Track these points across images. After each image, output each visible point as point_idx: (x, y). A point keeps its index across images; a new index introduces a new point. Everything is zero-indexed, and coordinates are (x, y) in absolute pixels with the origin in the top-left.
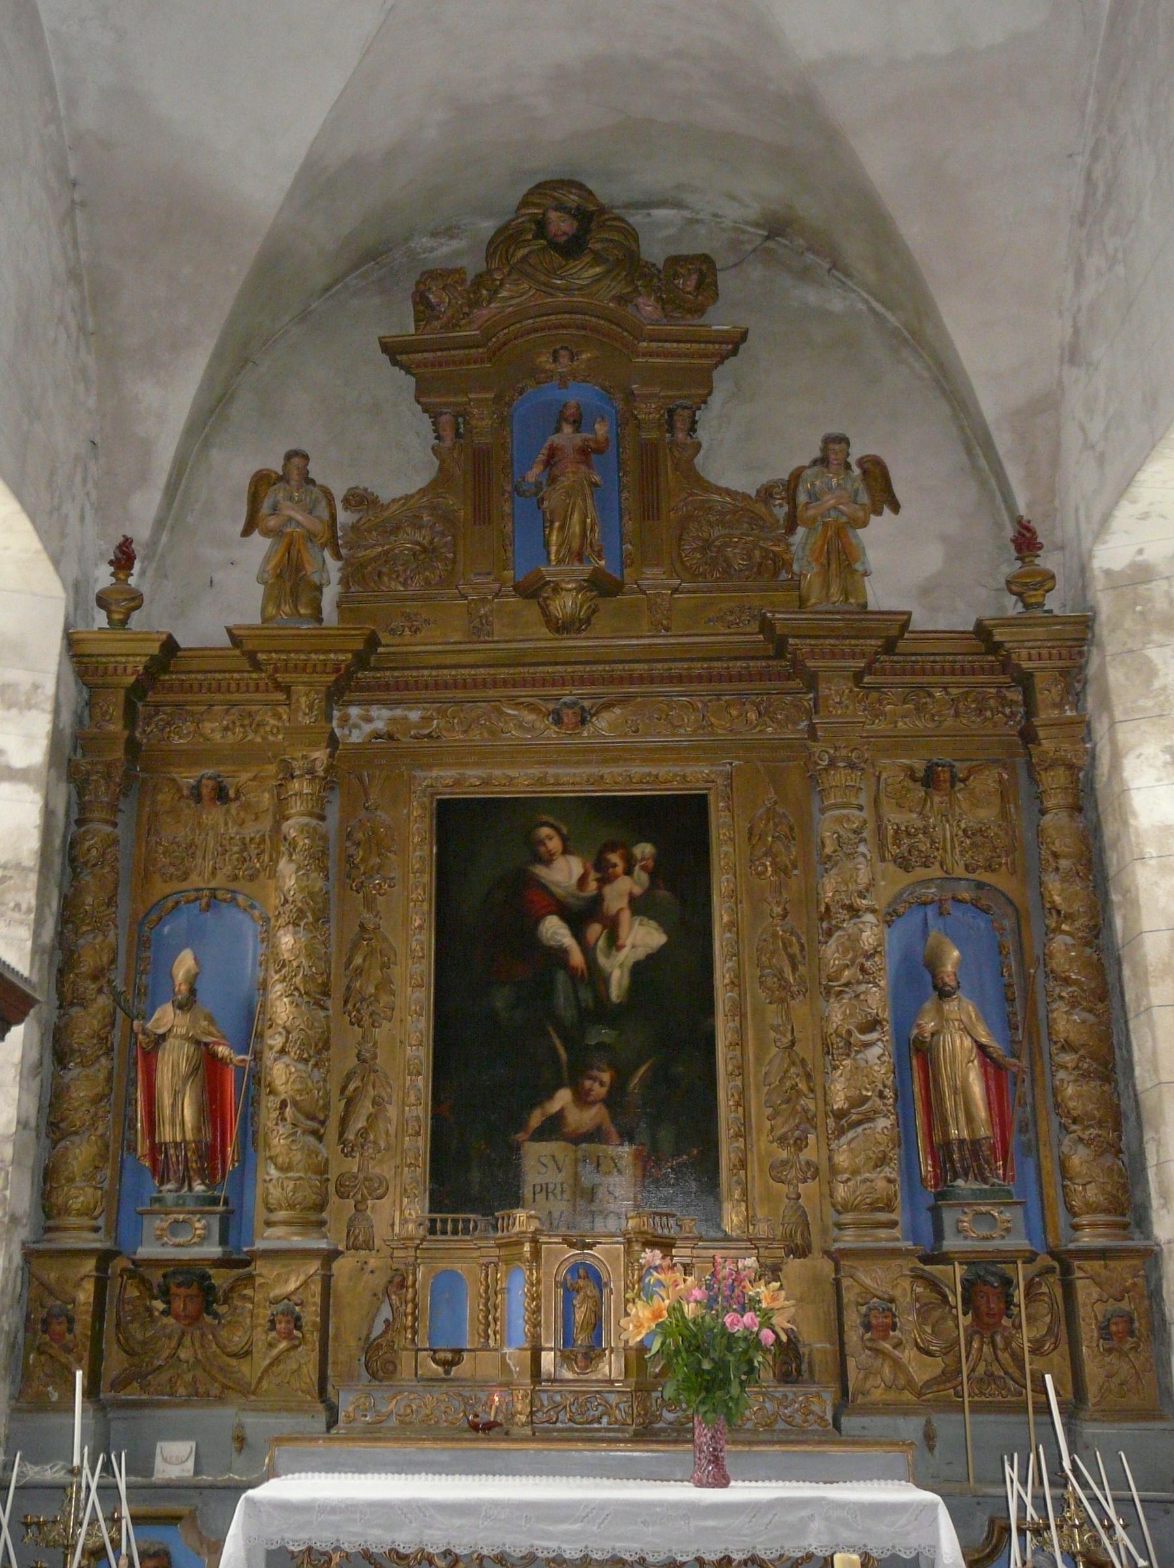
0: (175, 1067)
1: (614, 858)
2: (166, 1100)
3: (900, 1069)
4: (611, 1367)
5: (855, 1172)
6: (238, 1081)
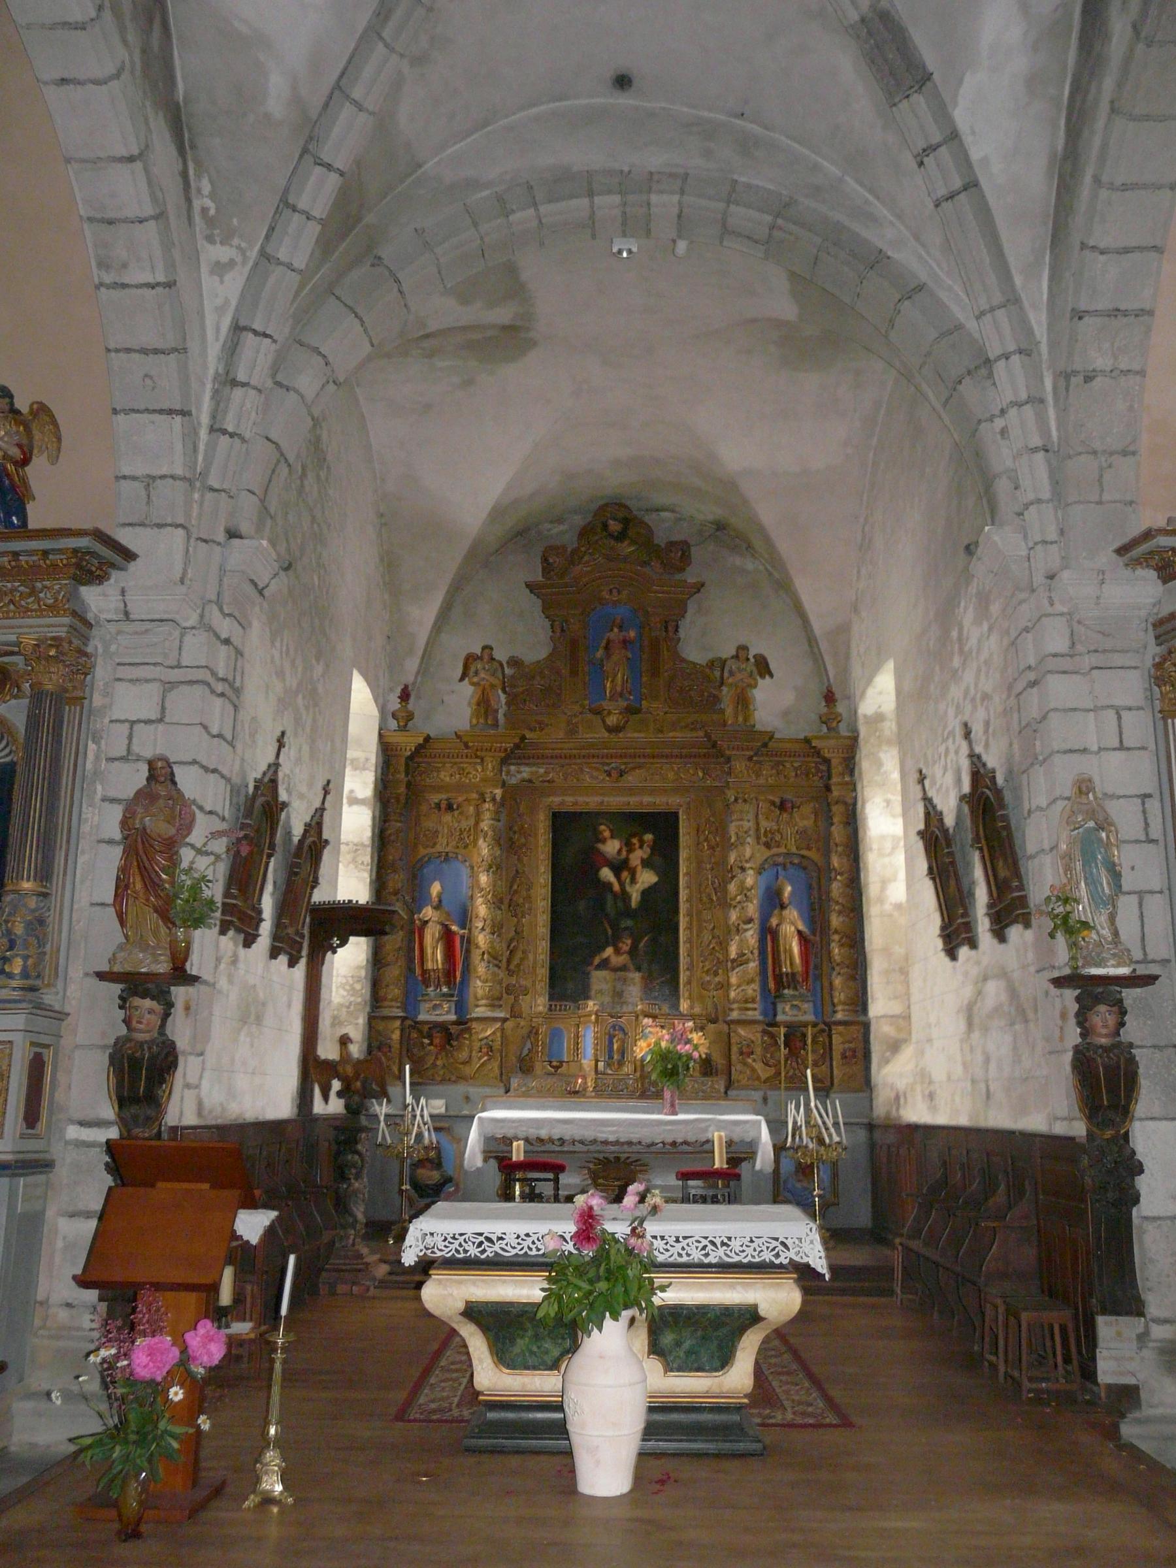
0: (433, 935)
1: (635, 841)
2: (429, 951)
3: (762, 941)
4: (627, 1069)
5: (739, 986)
6: (462, 943)
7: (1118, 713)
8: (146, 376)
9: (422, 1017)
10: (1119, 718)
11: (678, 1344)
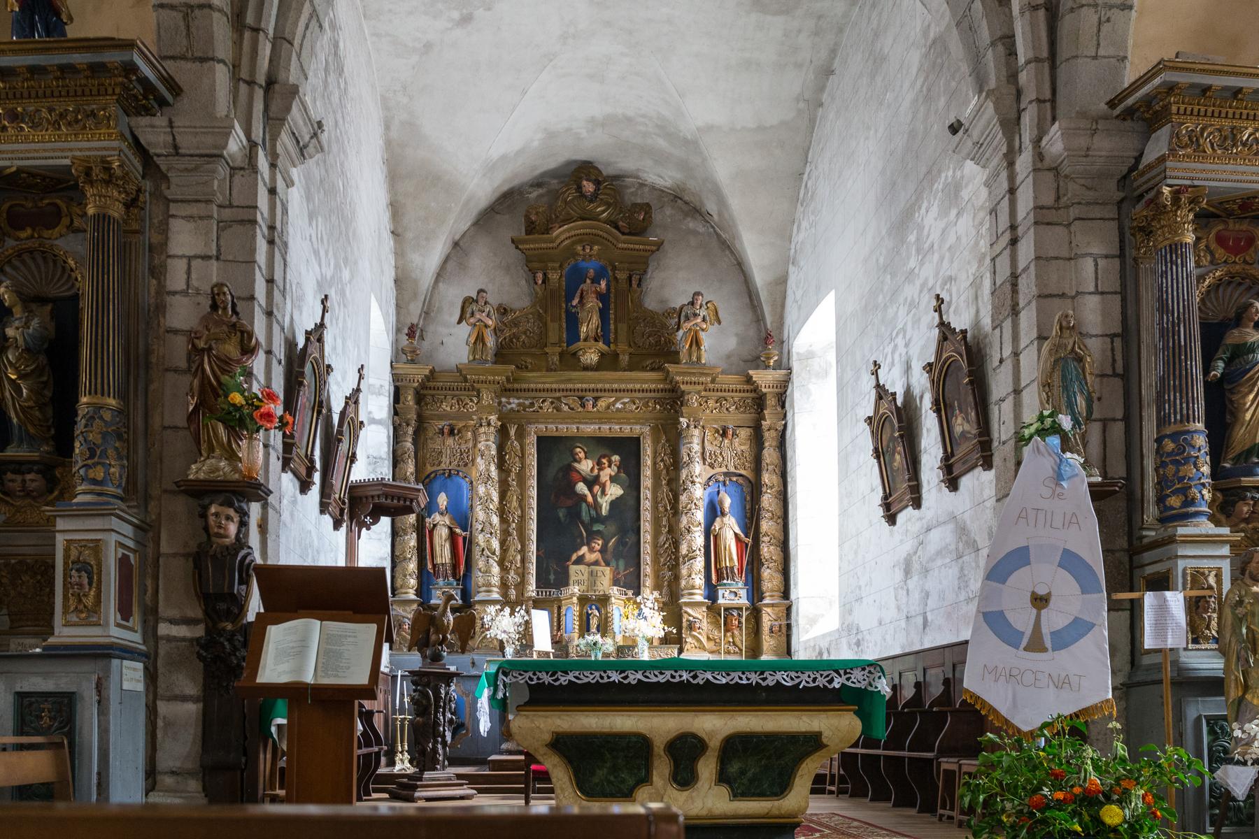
1: (604, 461)
2: (438, 549)
11: (742, 772)
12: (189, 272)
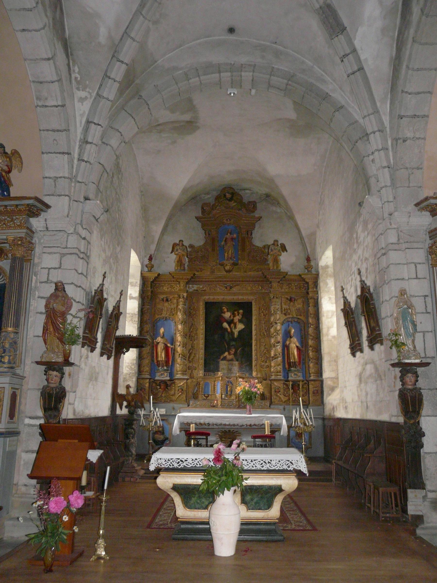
0: (161, 348)
1: (236, 313)
2: (159, 354)
3: (283, 350)
4: (233, 397)
5: (275, 367)
6: (172, 351)
7: (415, 265)
8: (54, 140)
9: (157, 378)
10: (416, 267)
11: (252, 500)
12: (48, 274)
